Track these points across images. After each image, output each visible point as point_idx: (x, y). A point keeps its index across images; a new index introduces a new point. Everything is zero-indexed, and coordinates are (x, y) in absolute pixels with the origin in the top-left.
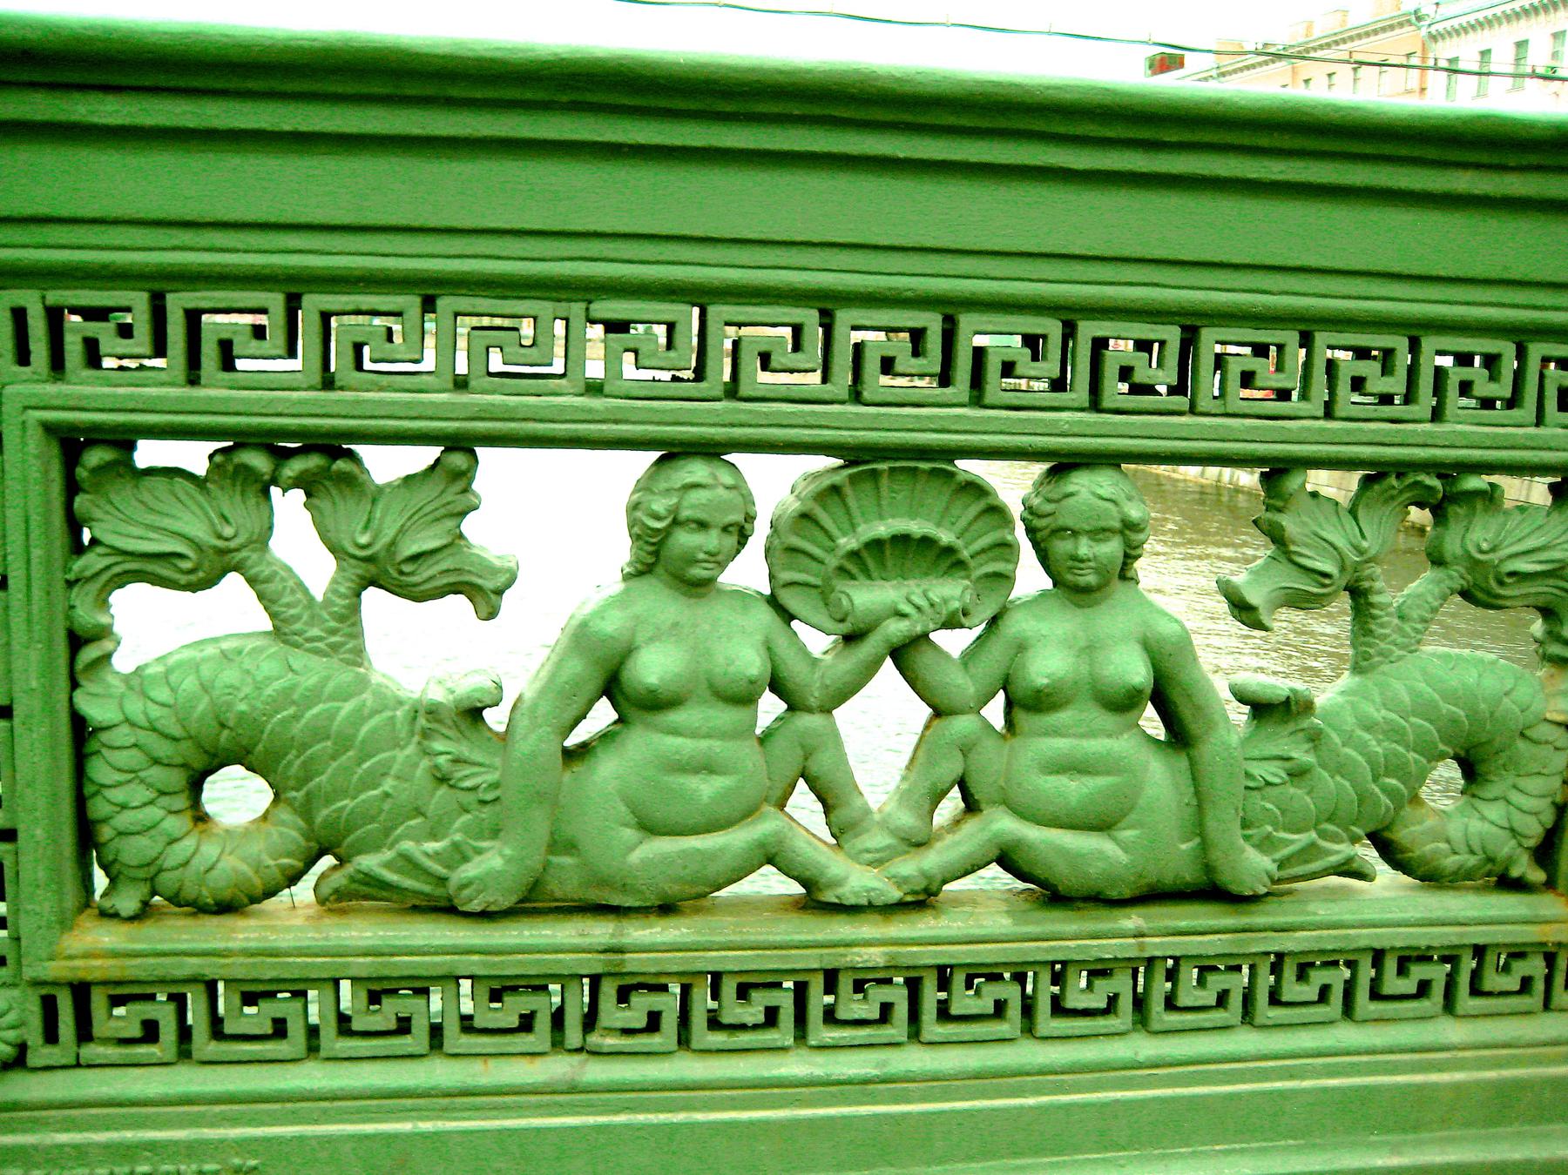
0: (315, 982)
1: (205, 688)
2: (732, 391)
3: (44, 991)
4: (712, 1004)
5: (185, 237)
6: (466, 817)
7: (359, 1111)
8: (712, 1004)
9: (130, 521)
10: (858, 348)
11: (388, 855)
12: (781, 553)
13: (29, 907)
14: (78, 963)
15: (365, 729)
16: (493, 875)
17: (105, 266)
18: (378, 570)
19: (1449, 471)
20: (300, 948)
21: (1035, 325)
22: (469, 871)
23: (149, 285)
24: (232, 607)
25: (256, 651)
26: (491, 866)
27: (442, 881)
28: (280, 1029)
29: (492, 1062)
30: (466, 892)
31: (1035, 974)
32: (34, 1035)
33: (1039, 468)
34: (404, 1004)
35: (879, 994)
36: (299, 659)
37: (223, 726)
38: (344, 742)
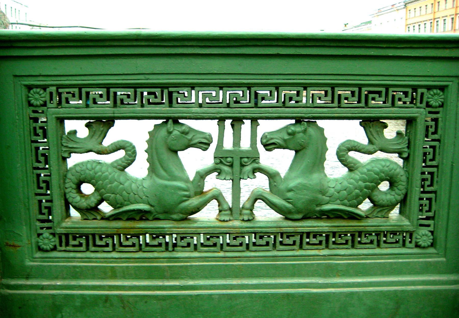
0: (141, 234)
4: (281, 239)
8: (281, 239)
20: (214, 226)
21: (326, 89)
28: (189, 245)
33: (231, 120)
34: (214, 240)
35: (320, 238)
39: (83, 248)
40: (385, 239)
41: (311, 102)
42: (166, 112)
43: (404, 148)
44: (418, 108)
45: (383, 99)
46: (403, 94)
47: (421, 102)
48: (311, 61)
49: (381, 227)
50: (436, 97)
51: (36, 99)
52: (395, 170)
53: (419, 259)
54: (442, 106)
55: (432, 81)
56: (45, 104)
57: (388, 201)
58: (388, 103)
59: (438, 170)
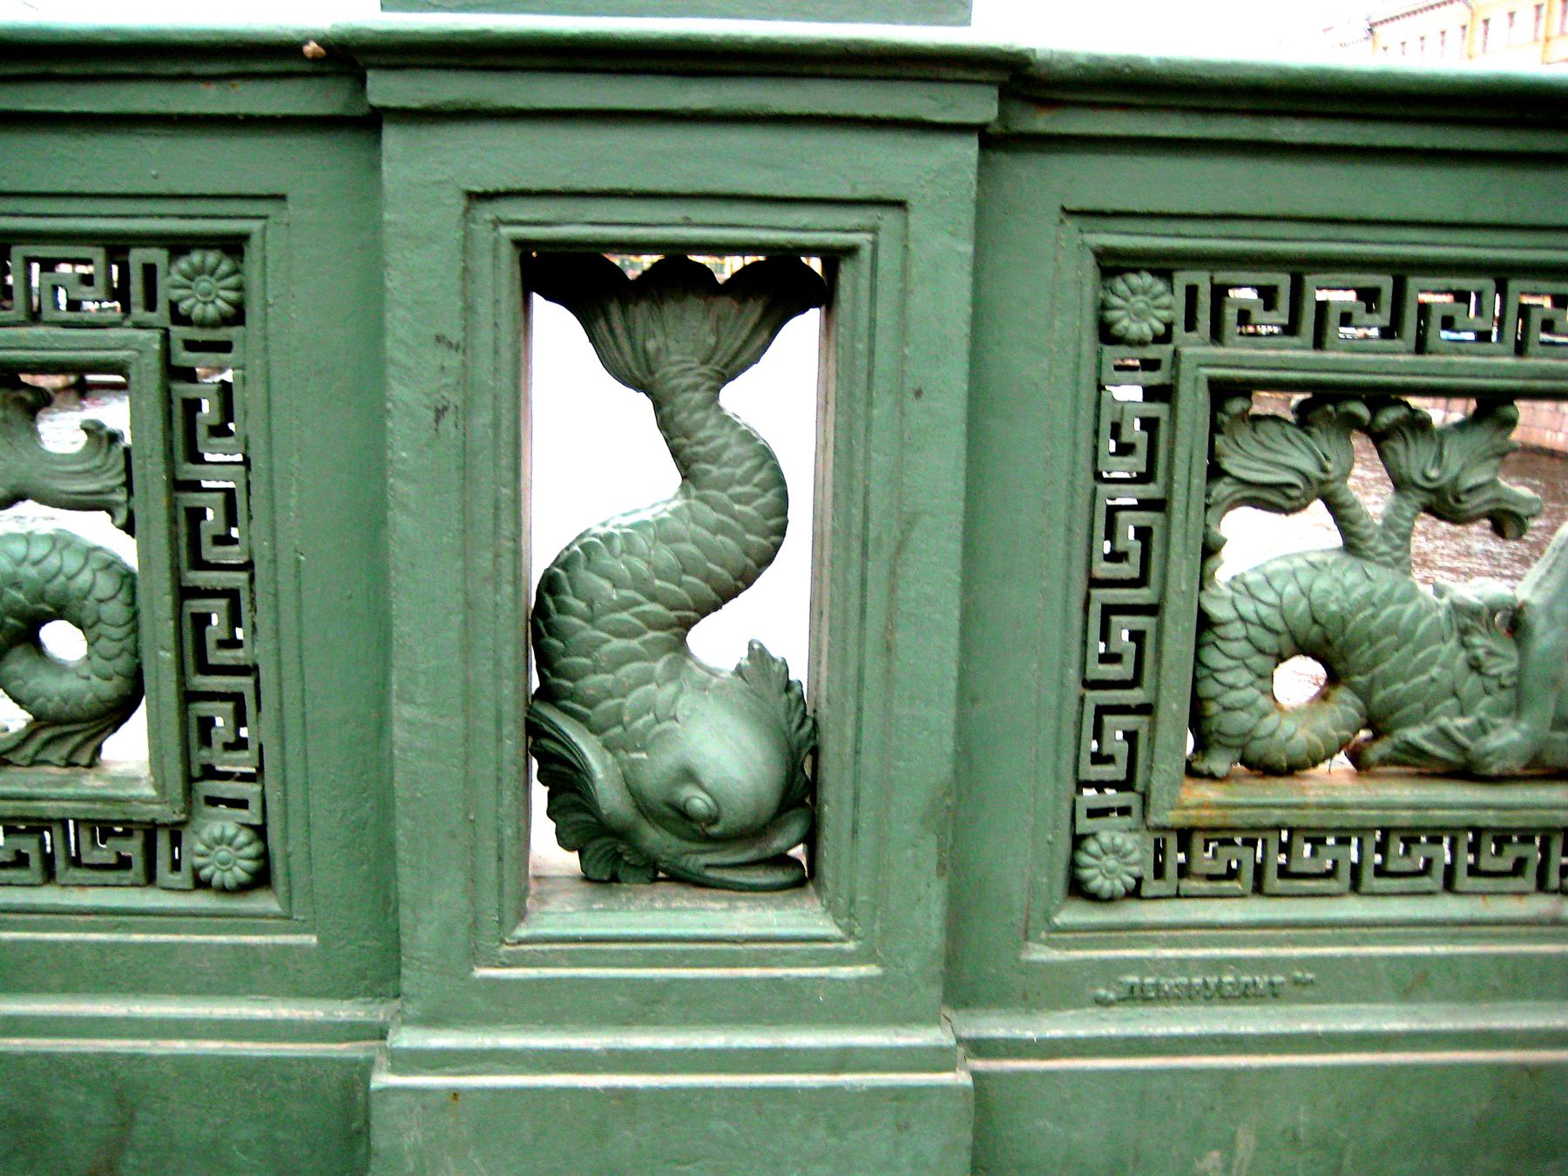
1: (1305, 593)
3: (1158, 835)
5: (1331, 231)
6: (1487, 700)
7: (1388, 936)
9: (1250, 457)
11: (1426, 729)
13: (1162, 766)
14: (1193, 812)
15: (1422, 627)
16: (1512, 745)
17: (1268, 254)
21: (1265, 278)
22: (1494, 741)
23: (1291, 269)
24: (1314, 528)
25: (1335, 563)
26: (1507, 738)
27: (1463, 749)
29: (1490, 899)
30: (1490, 759)
32: (1148, 873)
36: (1373, 570)
37: (1315, 621)
38: (1406, 636)
40: (1282, 859)
42: (1440, 370)
43: (113, 491)
44: (139, 326)
45: (1383, 318)
46: (1359, 297)
49: (43, 804)
50: (204, 283)
51: (1139, 316)
52: (70, 578)
53: (210, 933)
54: (237, 316)
55: (182, 217)
56: (1164, 338)
57: (66, 701)
58: (1400, 336)
59: (252, 579)
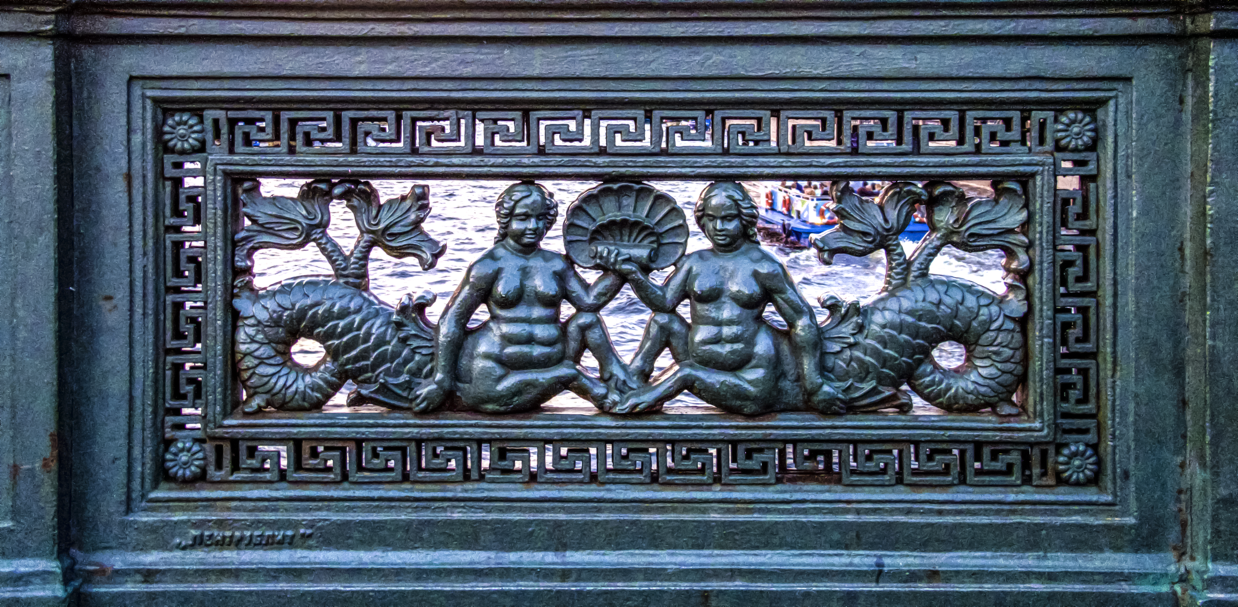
2: (978, 150)
10: (855, 128)
12: (569, 227)
18: (377, 238)
19: (933, 181)
31: (840, 452)
39: (1015, 478)
41: (790, 143)
47: (1042, 141)
48: (966, 50)
